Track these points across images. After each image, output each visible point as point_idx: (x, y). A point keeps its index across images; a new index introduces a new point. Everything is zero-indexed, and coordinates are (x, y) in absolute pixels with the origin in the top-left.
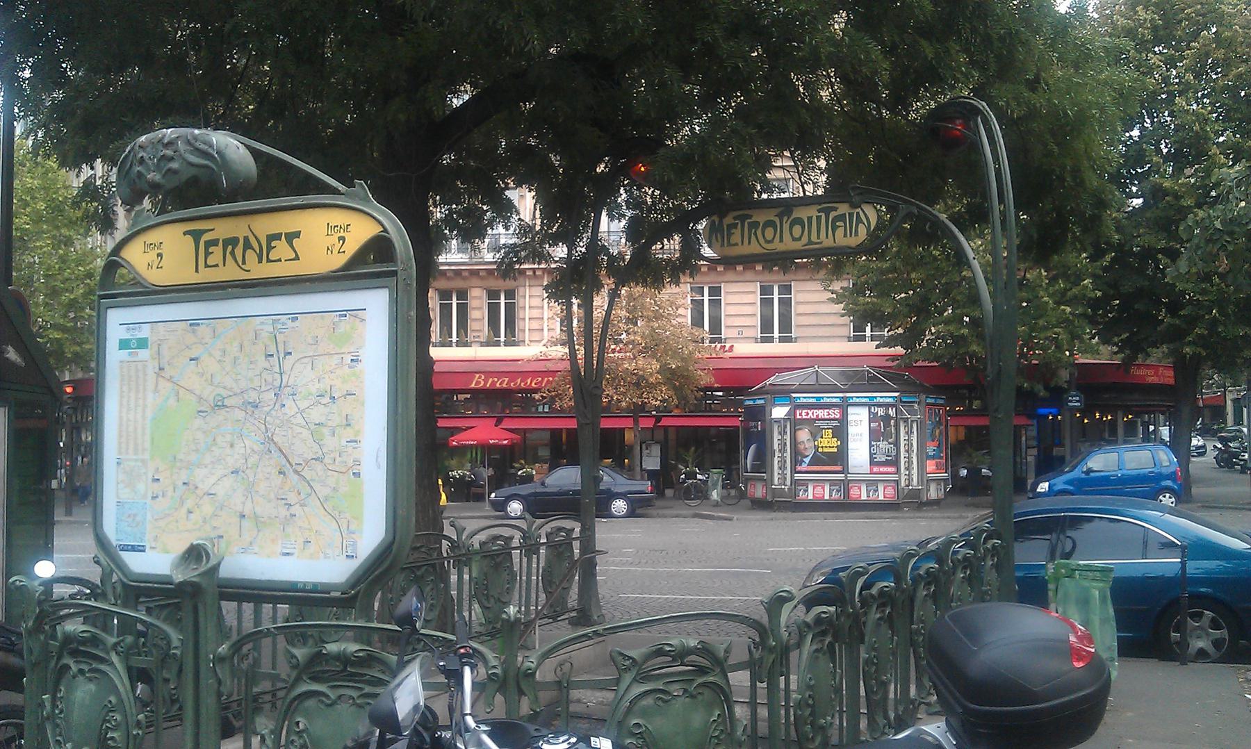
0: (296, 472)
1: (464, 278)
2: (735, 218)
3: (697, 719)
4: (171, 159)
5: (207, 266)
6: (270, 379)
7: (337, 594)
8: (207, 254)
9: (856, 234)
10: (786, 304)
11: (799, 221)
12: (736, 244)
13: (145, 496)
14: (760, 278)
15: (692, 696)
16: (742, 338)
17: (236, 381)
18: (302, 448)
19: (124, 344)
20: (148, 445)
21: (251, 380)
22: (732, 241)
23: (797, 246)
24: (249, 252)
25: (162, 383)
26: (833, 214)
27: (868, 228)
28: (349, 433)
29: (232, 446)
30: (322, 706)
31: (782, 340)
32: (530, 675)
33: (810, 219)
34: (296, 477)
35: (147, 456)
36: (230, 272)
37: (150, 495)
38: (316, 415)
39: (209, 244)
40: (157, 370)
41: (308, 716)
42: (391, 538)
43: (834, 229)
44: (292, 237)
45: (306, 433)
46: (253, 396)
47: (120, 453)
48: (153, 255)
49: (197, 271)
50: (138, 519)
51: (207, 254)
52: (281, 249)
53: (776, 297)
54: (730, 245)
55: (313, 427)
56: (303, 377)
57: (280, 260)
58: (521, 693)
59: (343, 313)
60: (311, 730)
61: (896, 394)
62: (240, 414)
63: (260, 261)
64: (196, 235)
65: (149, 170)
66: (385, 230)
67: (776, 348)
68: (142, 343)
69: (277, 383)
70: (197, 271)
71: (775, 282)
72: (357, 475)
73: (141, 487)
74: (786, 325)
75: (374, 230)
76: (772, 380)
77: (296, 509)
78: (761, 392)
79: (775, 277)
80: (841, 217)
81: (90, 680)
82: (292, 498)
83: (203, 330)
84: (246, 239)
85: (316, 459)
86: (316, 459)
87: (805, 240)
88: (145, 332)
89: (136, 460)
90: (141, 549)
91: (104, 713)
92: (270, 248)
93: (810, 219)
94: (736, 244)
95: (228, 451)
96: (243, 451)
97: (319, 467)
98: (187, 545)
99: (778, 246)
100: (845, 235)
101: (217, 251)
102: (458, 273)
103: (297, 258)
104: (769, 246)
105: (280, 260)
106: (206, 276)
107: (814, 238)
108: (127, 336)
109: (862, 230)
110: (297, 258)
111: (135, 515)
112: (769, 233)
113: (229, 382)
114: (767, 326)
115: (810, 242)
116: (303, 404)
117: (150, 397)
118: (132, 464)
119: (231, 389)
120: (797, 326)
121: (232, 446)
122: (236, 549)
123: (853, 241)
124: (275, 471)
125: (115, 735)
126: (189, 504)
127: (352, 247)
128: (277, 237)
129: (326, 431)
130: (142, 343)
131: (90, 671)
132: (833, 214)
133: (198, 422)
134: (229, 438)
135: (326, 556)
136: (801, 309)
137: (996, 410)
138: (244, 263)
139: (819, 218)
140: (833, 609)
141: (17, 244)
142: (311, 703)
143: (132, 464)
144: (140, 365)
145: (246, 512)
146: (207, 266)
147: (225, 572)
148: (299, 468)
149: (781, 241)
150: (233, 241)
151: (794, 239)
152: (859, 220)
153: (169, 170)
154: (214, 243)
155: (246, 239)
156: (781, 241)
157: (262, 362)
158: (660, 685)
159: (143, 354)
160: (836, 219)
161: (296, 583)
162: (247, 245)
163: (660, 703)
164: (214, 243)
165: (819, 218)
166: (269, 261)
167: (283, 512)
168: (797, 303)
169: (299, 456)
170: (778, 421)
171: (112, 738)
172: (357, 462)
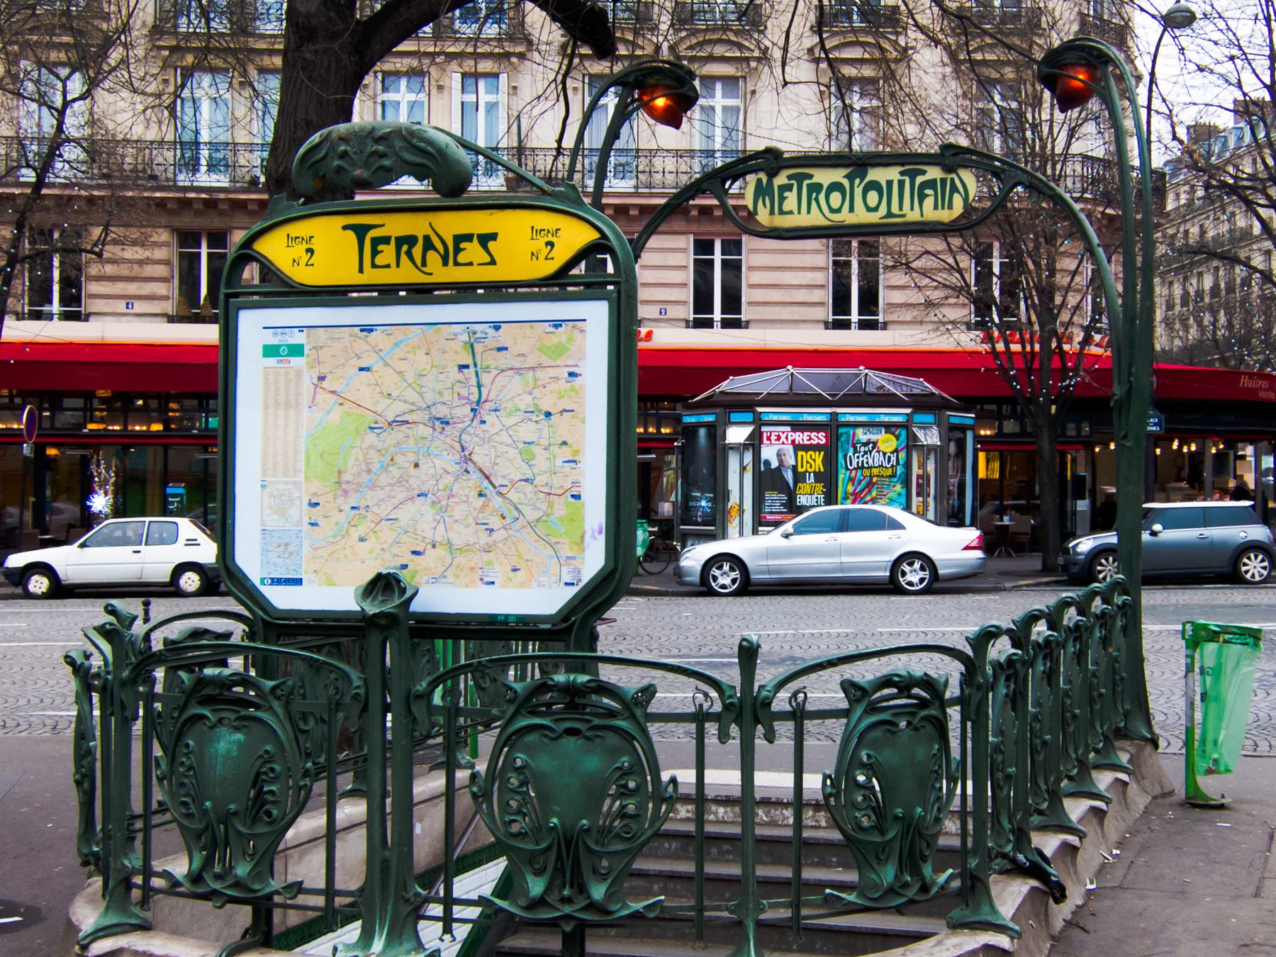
0: (500, 494)
1: (222, 213)
2: (789, 177)
3: (921, 753)
4: (383, 156)
5: (374, 266)
6: (464, 393)
7: (548, 626)
8: (375, 253)
9: (950, 207)
10: (733, 268)
12: (791, 212)
13: (300, 523)
14: (695, 228)
15: (916, 729)
16: (663, 319)
17: (420, 394)
18: (509, 469)
19: (270, 351)
20: (302, 465)
21: (440, 393)
22: (786, 208)
23: (873, 218)
24: (431, 254)
25: (321, 395)
26: (920, 179)
27: (966, 199)
28: (566, 453)
29: (416, 465)
30: (546, 741)
31: (726, 324)
32: (767, 703)
33: (890, 183)
34: (499, 500)
35: (301, 478)
36: (406, 274)
37: (306, 520)
38: (527, 431)
39: (376, 242)
40: (315, 381)
41: (528, 749)
42: (611, 567)
43: (922, 197)
44: (486, 240)
45: (512, 453)
46: (441, 411)
47: (264, 473)
49: (361, 270)
50: (291, 549)
51: (375, 253)
52: (472, 251)
53: (718, 257)
54: (782, 212)
55: (521, 446)
56: (509, 391)
57: (471, 264)
58: (757, 721)
59: (557, 324)
60: (532, 764)
61: (908, 411)
62: (427, 431)
63: (445, 263)
64: (360, 231)
65: (354, 165)
66: (604, 236)
67: (717, 338)
68: (297, 350)
69: (475, 397)
70: (361, 270)
71: (718, 235)
72: (577, 497)
73: (294, 513)
74: (732, 301)
75: (593, 235)
76: (725, 386)
77: (499, 535)
78: (708, 405)
79: (718, 228)
80: (931, 184)
81: (237, 729)
82: (495, 522)
83: (377, 335)
84: (427, 239)
85: (526, 480)
86: (526, 480)
87: (883, 210)
88: (298, 338)
89: (287, 483)
91: (260, 762)
92: (458, 250)
93: (890, 183)
94: (791, 212)
95: (412, 470)
96: (432, 471)
97: (528, 488)
98: (370, 576)
99: (846, 217)
100: (936, 208)
102: (211, 204)
103: (493, 262)
104: (836, 218)
105: (471, 264)
106: (372, 276)
107: (895, 210)
108: (275, 341)
109: (958, 201)
110: (493, 262)
111: (287, 545)
112: (836, 198)
113: (411, 395)
114: (703, 301)
115: (890, 214)
116: (509, 422)
117: (305, 413)
118: (281, 487)
119: (413, 404)
120: (750, 303)
121: (416, 465)
122: (425, 579)
123: (945, 216)
124: (474, 493)
125: (274, 788)
126: (362, 530)
127: (562, 255)
128: (468, 238)
129: (537, 450)
130: (297, 350)
131: (236, 719)
132: (920, 179)
133: (371, 438)
134: (412, 458)
135: (540, 585)
136: (756, 277)
137: (1125, 437)
138: (424, 264)
139: (901, 183)
142: (531, 738)
143: (281, 487)
144: (292, 375)
145: (438, 539)
146: (374, 266)
147: (417, 606)
148: (504, 490)
149: (852, 209)
150: (411, 240)
151: (869, 209)
152: (954, 189)
153: (381, 168)
154: (386, 240)
155: (427, 239)
156: (852, 209)
157: (455, 374)
158: (885, 716)
159: (296, 361)
160: (924, 185)
161: (496, 616)
162: (428, 245)
163: (888, 735)
164: (386, 240)
165: (901, 183)
166: (456, 264)
167: (484, 538)
168: (751, 268)
169: (503, 477)
170: (735, 447)
171: (272, 792)
172: (575, 483)
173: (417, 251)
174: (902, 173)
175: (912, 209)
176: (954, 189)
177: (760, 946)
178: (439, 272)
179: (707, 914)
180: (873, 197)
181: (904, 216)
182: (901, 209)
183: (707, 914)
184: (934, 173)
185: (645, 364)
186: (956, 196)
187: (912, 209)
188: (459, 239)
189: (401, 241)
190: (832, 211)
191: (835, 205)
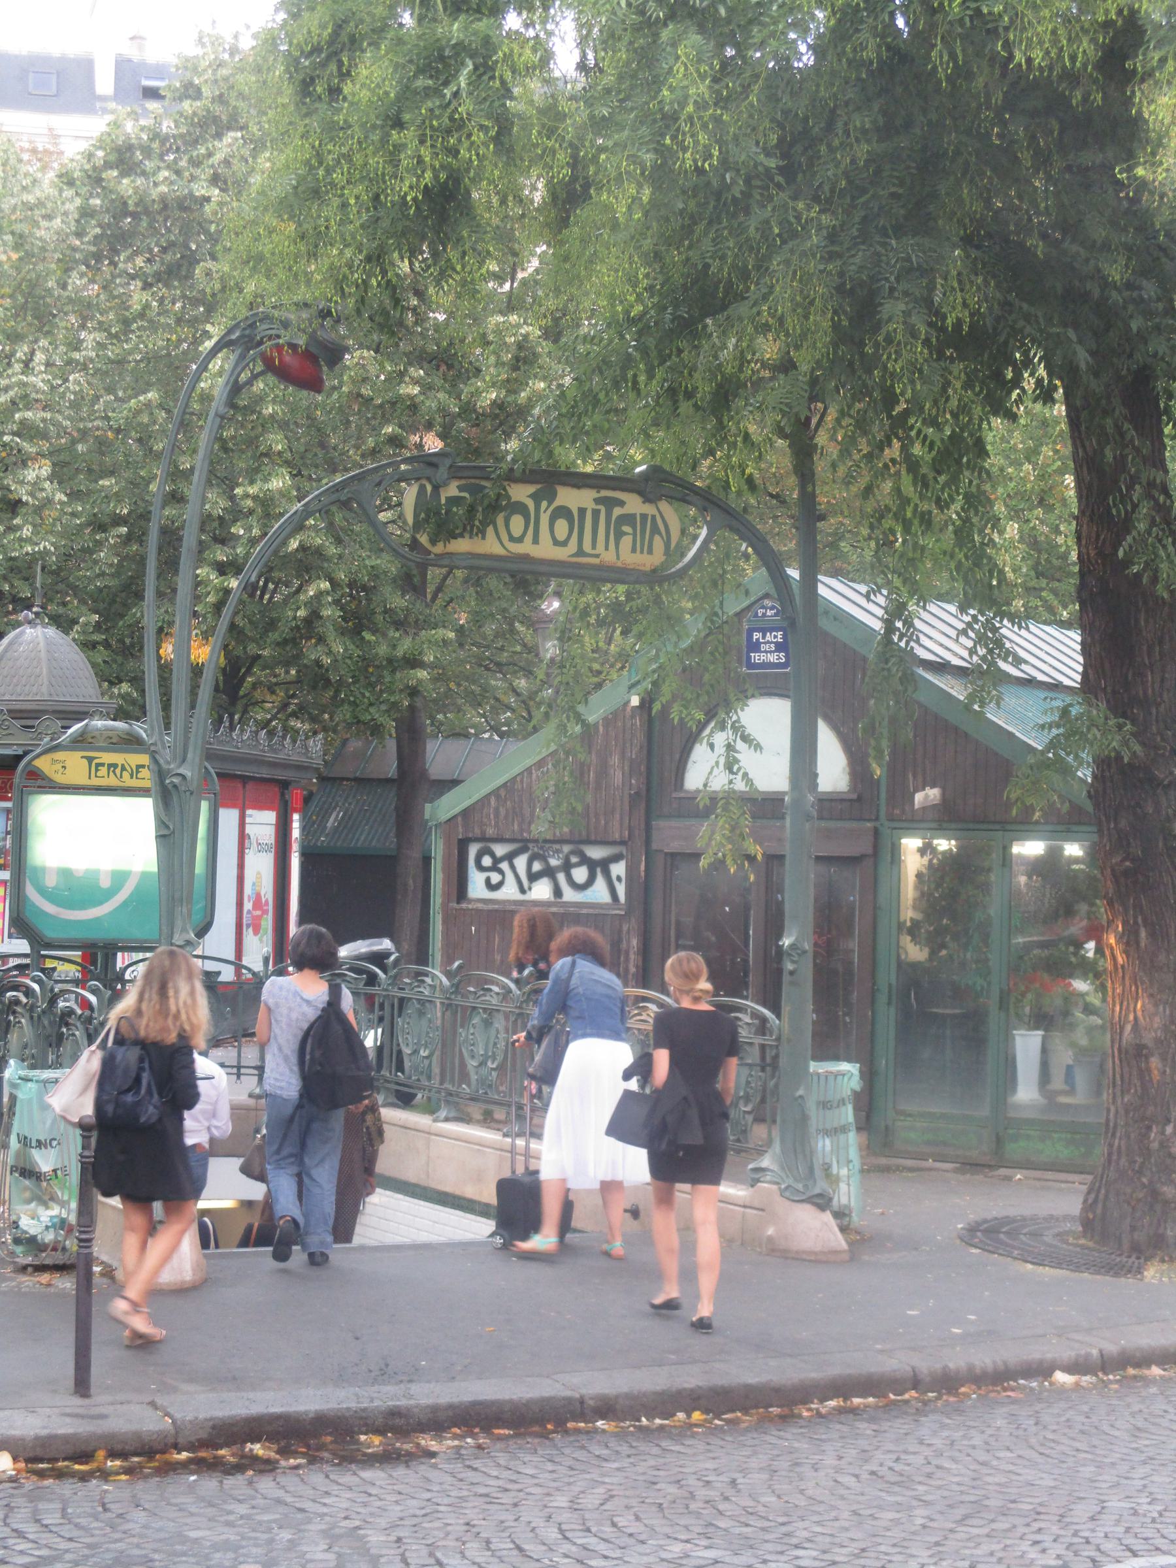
2: (460, 488)
9: (650, 552)
11: (563, 512)
23: (561, 554)
26: (617, 511)
36: (112, 781)
39: (98, 765)
43: (619, 535)
48: (58, 766)
64: (90, 760)
80: (628, 519)
87: (573, 546)
90: (758, 747)
93: (582, 511)
100: (634, 550)
101: (103, 771)
106: (96, 782)
107: (587, 547)
115: (580, 552)
132: (617, 511)
139: (596, 513)
140: (296, 817)
141: (786, 978)
149: (536, 541)
150: (115, 766)
151: (556, 543)
152: (655, 530)
154: (103, 765)
156: (536, 541)
162: (123, 769)
165: (596, 513)
173: (118, 771)
174: (597, 501)
175: (607, 549)
176: (655, 530)
177: (86, 66)
178: (128, 782)
179: (204, 806)
180: (562, 526)
181: (597, 556)
182: (594, 547)
183: (204, 806)
184: (634, 504)
185: (71, 1382)
186: (657, 538)
187: (607, 549)
188: (139, 767)
189: (110, 766)
190: (512, 539)
191: (517, 533)
